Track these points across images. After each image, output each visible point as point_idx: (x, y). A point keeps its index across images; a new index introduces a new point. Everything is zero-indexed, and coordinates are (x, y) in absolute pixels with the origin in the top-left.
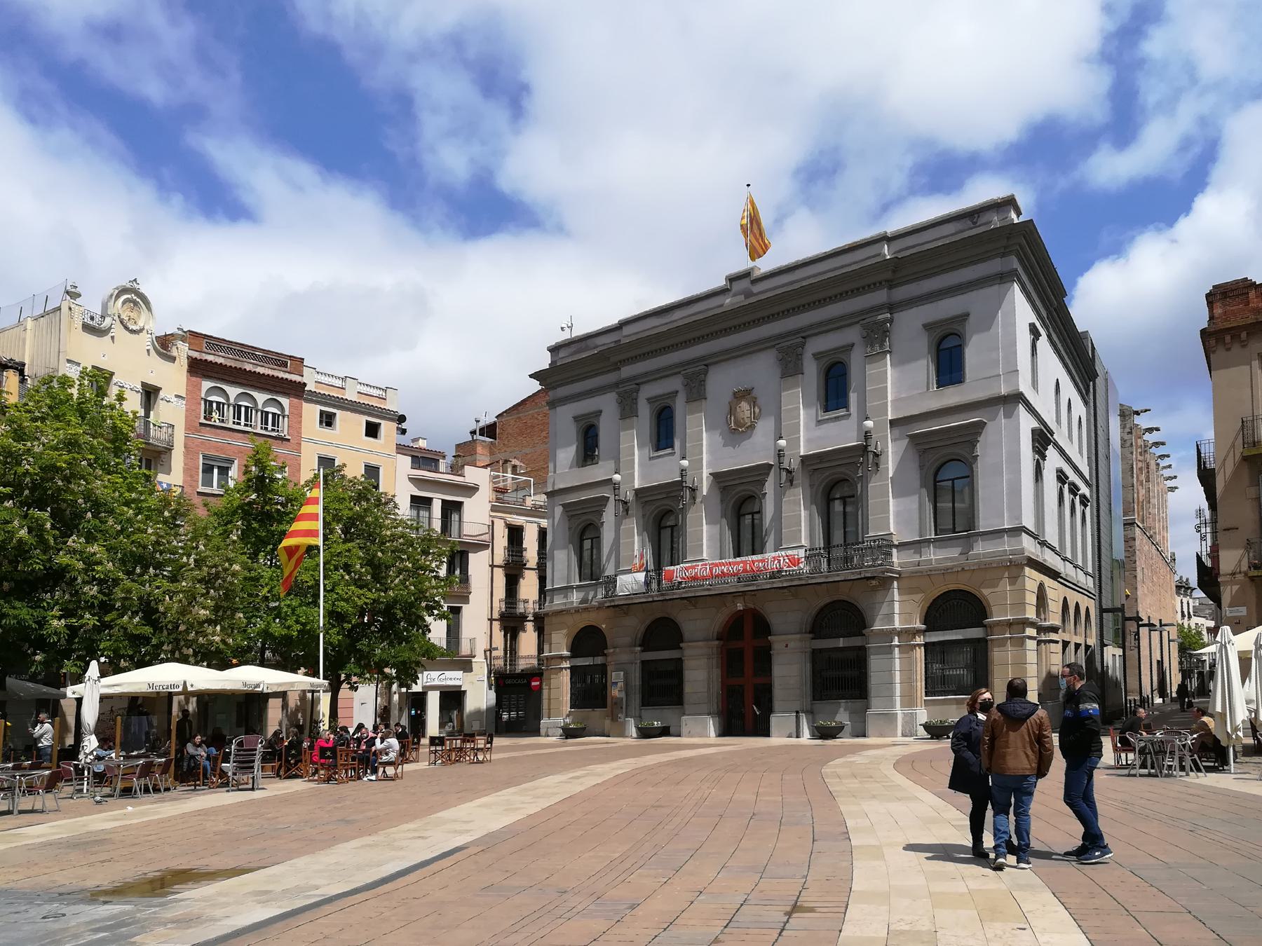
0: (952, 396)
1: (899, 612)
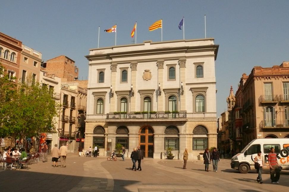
0: (200, 80)
1: (187, 130)
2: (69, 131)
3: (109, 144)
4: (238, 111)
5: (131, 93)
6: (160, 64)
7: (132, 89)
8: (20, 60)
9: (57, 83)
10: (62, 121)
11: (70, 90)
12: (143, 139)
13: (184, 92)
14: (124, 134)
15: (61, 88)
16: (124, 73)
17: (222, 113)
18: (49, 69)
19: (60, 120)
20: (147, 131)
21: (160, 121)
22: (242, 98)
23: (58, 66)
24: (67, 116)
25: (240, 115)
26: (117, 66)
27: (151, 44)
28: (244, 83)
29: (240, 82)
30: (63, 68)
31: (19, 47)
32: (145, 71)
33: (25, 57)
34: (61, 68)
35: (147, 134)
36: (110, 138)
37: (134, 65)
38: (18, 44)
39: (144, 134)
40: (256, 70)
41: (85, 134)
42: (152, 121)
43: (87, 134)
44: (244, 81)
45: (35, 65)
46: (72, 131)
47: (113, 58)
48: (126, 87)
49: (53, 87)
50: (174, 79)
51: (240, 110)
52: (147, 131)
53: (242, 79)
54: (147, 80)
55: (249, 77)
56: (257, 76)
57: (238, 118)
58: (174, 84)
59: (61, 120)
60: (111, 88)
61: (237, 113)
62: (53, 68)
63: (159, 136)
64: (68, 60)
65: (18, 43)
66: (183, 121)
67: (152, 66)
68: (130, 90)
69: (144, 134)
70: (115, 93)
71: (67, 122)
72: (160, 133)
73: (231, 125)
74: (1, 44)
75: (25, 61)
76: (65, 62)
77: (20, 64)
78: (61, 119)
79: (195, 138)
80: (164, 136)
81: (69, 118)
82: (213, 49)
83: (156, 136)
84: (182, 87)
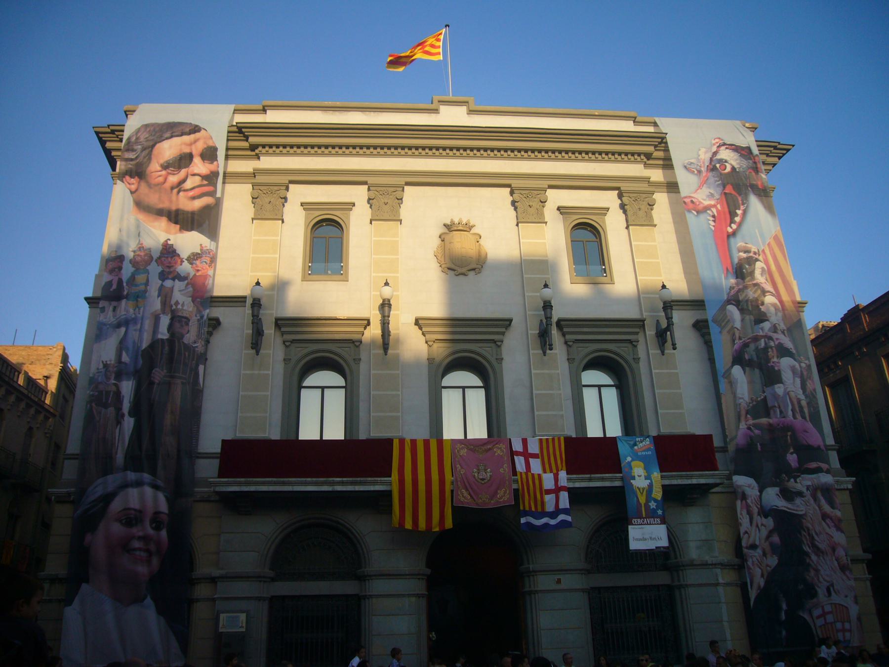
37: (386, 198)
54: (460, 270)
79: (284, 597)
80: (378, 586)
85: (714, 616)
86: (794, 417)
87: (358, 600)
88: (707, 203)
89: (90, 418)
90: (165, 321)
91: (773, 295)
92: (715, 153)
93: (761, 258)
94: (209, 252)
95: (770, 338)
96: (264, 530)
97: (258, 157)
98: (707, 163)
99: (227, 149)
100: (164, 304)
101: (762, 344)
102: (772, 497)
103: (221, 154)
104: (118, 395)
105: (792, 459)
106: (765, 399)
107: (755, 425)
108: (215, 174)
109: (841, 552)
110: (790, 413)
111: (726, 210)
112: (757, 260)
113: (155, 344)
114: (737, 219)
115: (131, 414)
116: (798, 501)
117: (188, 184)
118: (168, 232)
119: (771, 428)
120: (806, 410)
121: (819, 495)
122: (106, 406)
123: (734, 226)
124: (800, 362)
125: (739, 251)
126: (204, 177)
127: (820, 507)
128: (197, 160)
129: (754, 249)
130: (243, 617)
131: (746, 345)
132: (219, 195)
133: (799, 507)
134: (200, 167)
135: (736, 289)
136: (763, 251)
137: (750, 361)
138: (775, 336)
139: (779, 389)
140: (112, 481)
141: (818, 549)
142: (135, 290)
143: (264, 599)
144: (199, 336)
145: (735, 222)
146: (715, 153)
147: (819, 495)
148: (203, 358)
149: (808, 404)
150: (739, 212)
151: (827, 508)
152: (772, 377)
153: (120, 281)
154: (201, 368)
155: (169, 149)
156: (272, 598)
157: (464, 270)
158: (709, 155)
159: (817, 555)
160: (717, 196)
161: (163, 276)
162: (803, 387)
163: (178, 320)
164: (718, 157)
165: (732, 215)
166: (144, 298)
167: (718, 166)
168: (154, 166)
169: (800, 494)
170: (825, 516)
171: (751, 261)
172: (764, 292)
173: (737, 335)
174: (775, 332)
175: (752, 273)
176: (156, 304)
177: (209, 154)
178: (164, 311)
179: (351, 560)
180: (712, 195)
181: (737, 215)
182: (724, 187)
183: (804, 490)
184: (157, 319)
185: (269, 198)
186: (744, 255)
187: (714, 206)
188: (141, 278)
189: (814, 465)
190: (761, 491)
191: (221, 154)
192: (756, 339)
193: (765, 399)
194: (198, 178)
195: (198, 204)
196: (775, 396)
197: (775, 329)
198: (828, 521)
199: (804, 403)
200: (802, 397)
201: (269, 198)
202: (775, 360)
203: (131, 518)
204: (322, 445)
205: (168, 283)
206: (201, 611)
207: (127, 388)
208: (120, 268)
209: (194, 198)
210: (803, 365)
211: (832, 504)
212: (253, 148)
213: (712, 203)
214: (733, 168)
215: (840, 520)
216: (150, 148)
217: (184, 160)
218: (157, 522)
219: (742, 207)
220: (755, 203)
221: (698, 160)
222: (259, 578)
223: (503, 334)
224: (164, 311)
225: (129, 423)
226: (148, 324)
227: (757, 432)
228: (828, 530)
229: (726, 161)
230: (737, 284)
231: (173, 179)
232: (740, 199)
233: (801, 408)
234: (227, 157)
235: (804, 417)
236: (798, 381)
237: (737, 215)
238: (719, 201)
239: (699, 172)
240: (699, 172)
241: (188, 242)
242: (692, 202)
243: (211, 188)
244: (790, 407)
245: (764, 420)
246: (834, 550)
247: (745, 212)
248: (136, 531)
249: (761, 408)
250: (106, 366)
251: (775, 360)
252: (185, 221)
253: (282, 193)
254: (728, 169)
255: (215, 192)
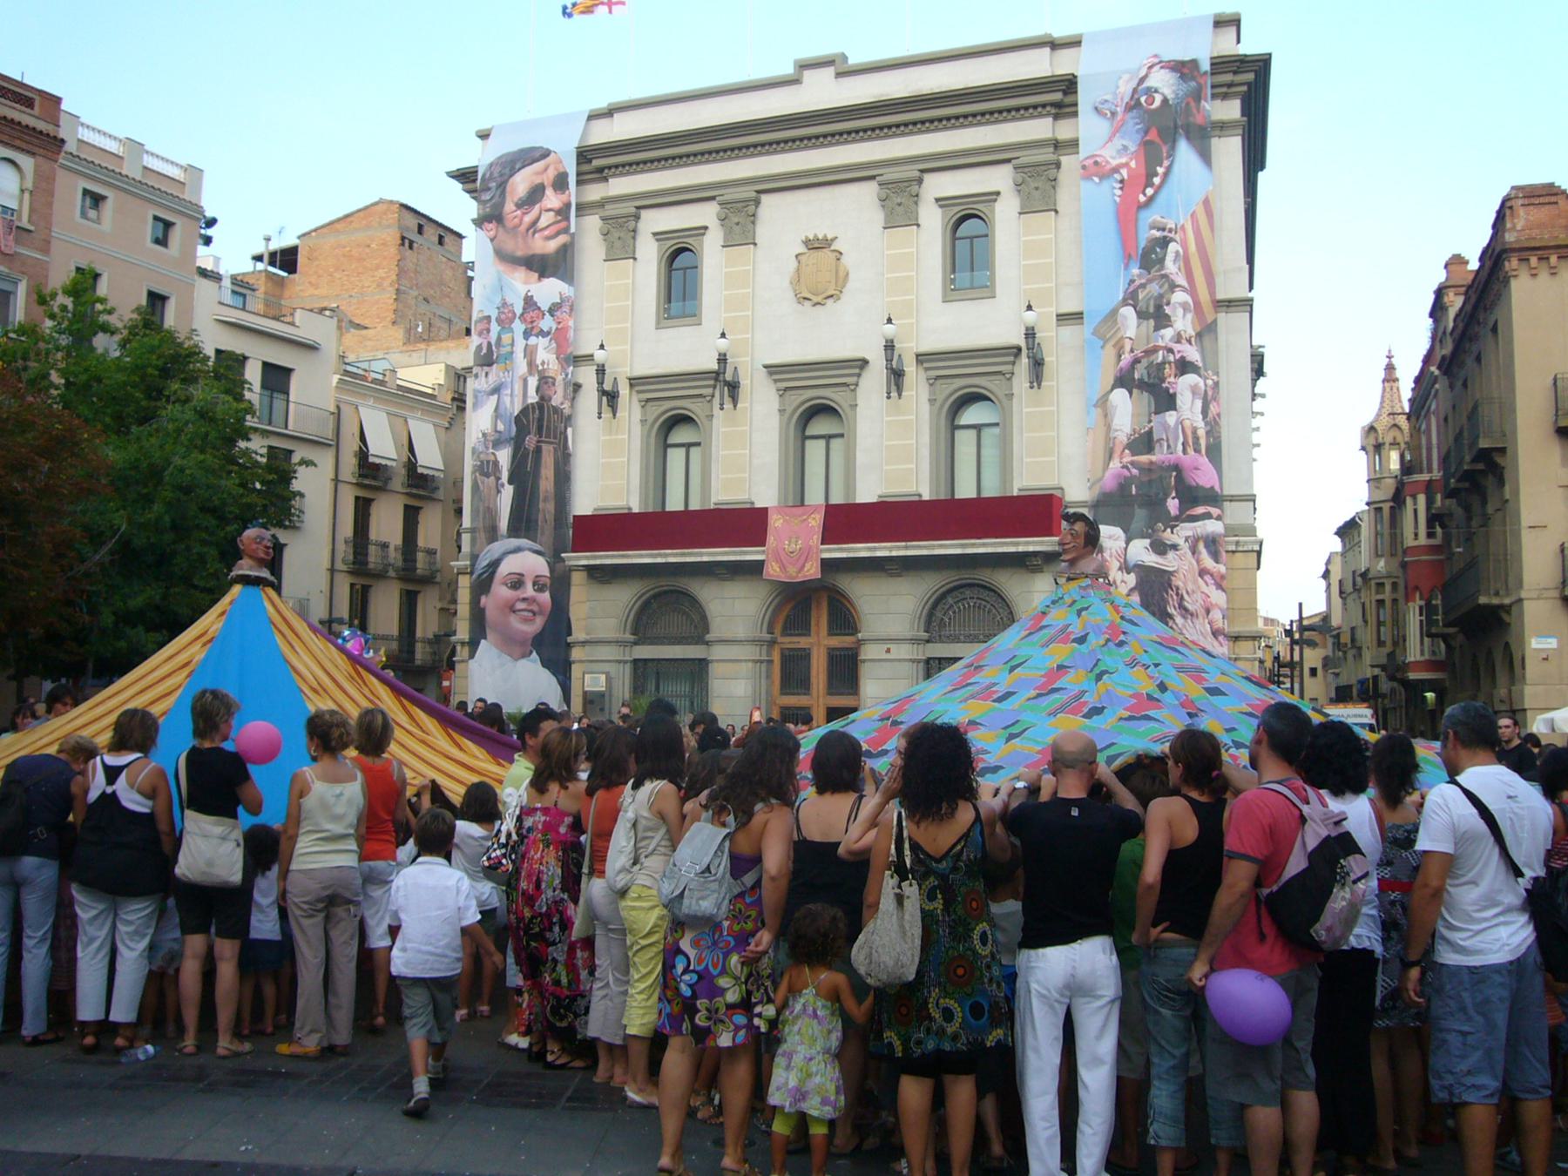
2: (395, 632)
3: (591, 702)
4: (1422, 498)
5: (723, 382)
6: (899, 194)
7: (722, 359)
8: (55, 206)
9: (311, 348)
10: (350, 572)
11: (400, 387)
12: (794, 672)
13: (1046, 369)
14: (679, 643)
15: (336, 378)
16: (679, 257)
17: (1341, 523)
18: (313, 280)
19: (339, 565)
20: (820, 618)
21: (894, 553)
22: (1442, 417)
23: (360, 260)
24: (385, 546)
25: (1433, 519)
26: (642, 225)
27: (839, 75)
28: (1452, 313)
29: (1432, 315)
30: (388, 272)
31: (41, 125)
32: (807, 242)
33: (86, 192)
34: (381, 273)
35: (819, 643)
36: (595, 667)
37: (740, 211)
38: (37, 111)
39: (802, 642)
40: (1522, 212)
41: (459, 648)
42: (844, 555)
43: (584, 643)
44: (1455, 302)
45: (162, 241)
46: (419, 634)
47: (614, 175)
48: (687, 350)
49: (288, 372)
50: (985, 292)
51: (1429, 488)
52: (820, 618)
53: (1440, 293)
54: (815, 299)
55: (1536, 928)
56: (1533, 244)
57: (1423, 540)
58: (987, 323)
59: (345, 568)
60: (600, 356)
61: (1415, 511)
62: (337, 275)
63: (888, 651)
64: (441, 237)
65: (37, 104)
66: (1035, 554)
67: (851, 214)
68: (716, 367)
69: (802, 642)
70: (624, 390)
71: (381, 575)
72: (741, 632)
73: (1388, 588)
74: (6, 144)
75: (92, 214)
76: (403, 238)
77: (56, 231)
78: (344, 561)
79: (646, 661)
80: (717, 652)
81: (395, 557)
82: (1230, 85)
83: (869, 652)
84: (1030, 334)
85: (108, 731)
86: (1185, 451)
87: (702, 665)
88: (1114, 163)
89: (475, 488)
90: (533, 382)
91: (1184, 290)
92: (1142, 80)
93: (1177, 237)
94: (568, 298)
95: (1170, 351)
96: (623, 597)
97: (606, 179)
98: (1127, 99)
99: (578, 174)
100: (531, 365)
101: (1160, 356)
102: (1140, 551)
103: (572, 180)
104: (496, 463)
105: (1173, 505)
106: (1150, 432)
107: (1132, 463)
108: (568, 205)
109: (1217, 615)
110: (1180, 447)
111: (1143, 171)
112: (1172, 240)
113: (525, 411)
114: (1157, 180)
115: (510, 482)
116: (1171, 554)
117: (543, 223)
118: (526, 283)
119: (1149, 469)
120: (1203, 442)
121: (1201, 546)
122: (487, 475)
123: (1150, 191)
124: (1205, 379)
125: (1152, 228)
126: (558, 212)
127: (1198, 562)
128: (549, 192)
129: (1171, 225)
130: (603, 677)
131: (1137, 361)
132: (573, 230)
133: (1169, 562)
134: (552, 200)
135: (1137, 283)
136: (1183, 228)
137: (1141, 380)
138: (1176, 347)
139: (1171, 418)
140: (497, 548)
141: (1186, 610)
142: (504, 350)
143: (625, 662)
144: (565, 397)
145: (1152, 185)
146: (1142, 80)
147: (1201, 546)
148: (568, 420)
149: (1208, 433)
150: (1160, 170)
151: (1208, 562)
152: (1166, 401)
153: (489, 344)
154: (569, 430)
155: (521, 183)
156: (636, 661)
157: (819, 299)
158: (1134, 84)
159: (1184, 617)
160: (1133, 148)
161: (527, 334)
162: (1205, 412)
163: (545, 381)
164: (1146, 84)
165: (1151, 174)
166: (512, 360)
167: (1143, 99)
168: (509, 206)
169: (1175, 547)
170: (1203, 572)
171: (1164, 243)
172: (1173, 287)
173: (1128, 348)
174: (1178, 342)
175: (1162, 261)
176: (521, 365)
177: (560, 183)
178: (530, 373)
179: (698, 628)
180: (1125, 148)
181: (1156, 174)
182: (1146, 133)
183: (1181, 542)
184: (525, 381)
185: (621, 231)
186: (1158, 234)
187: (1126, 165)
188: (506, 338)
189: (1200, 510)
190: (1127, 543)
191: (572, 180)
192: (1155, 350)
193: (1150, 432)
194: (552, 214)
195: (552, 246)
196: (1165, 427)
197: (1178, 338)
198: (1208, 578)
199: (1201, 433)
200: (1200, 424)
201: (621, 231)
202: (1172, 379)
203: (517, 582)
204: (687, 515)
205: (533, 340)
206: (576, 670)
207: (504, 456)
208: (488, 331)
209: (549, 238)
210: (1210, 382)
211: (1216, 556)
212: (600, 170)
213: (1123, 160)
214: (1165, 101)
215: (1223, 577)
216: (502, 186)
217: (536, 193)
218: (539, 586)
219: (1166, 163)
220: (1185, 152)
221: (1115, 94)
222: (617, 642)
223: (859, 375)
224: (530, 373)
225: (508, 492)
226: (518, 387)
227: (1135, 471)
228: (1204, 588)
229: (1156, 91)
230: (1140, 276)
231: (528, 219)
232: (1165, 150)
233: (1196, 439)
234: (579, 183)
235: (1197, 451)
236: (1199, 404)
237: (1156, 174)
238: (1135, 155)
239: (1113, 114)
240: (1113, 114)
241: (549, 290)
242: (1096, 163)
243: (563, 224)
244: (1181, 440)
245: (1144, 458)
246: (1208, 611)
247: (1166, 175)
248: (520, 594)
249: (1144, 442)
250: (484, 435)
251: (1172, 379)
252: (542, 266)
253: (632, 224)
254: (1157, 103)
255: (568, 228)
